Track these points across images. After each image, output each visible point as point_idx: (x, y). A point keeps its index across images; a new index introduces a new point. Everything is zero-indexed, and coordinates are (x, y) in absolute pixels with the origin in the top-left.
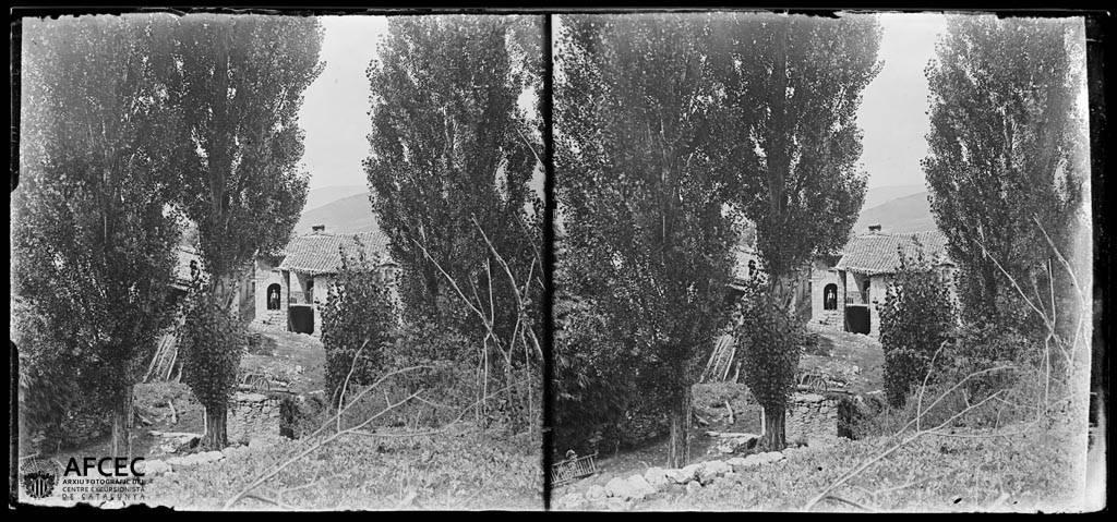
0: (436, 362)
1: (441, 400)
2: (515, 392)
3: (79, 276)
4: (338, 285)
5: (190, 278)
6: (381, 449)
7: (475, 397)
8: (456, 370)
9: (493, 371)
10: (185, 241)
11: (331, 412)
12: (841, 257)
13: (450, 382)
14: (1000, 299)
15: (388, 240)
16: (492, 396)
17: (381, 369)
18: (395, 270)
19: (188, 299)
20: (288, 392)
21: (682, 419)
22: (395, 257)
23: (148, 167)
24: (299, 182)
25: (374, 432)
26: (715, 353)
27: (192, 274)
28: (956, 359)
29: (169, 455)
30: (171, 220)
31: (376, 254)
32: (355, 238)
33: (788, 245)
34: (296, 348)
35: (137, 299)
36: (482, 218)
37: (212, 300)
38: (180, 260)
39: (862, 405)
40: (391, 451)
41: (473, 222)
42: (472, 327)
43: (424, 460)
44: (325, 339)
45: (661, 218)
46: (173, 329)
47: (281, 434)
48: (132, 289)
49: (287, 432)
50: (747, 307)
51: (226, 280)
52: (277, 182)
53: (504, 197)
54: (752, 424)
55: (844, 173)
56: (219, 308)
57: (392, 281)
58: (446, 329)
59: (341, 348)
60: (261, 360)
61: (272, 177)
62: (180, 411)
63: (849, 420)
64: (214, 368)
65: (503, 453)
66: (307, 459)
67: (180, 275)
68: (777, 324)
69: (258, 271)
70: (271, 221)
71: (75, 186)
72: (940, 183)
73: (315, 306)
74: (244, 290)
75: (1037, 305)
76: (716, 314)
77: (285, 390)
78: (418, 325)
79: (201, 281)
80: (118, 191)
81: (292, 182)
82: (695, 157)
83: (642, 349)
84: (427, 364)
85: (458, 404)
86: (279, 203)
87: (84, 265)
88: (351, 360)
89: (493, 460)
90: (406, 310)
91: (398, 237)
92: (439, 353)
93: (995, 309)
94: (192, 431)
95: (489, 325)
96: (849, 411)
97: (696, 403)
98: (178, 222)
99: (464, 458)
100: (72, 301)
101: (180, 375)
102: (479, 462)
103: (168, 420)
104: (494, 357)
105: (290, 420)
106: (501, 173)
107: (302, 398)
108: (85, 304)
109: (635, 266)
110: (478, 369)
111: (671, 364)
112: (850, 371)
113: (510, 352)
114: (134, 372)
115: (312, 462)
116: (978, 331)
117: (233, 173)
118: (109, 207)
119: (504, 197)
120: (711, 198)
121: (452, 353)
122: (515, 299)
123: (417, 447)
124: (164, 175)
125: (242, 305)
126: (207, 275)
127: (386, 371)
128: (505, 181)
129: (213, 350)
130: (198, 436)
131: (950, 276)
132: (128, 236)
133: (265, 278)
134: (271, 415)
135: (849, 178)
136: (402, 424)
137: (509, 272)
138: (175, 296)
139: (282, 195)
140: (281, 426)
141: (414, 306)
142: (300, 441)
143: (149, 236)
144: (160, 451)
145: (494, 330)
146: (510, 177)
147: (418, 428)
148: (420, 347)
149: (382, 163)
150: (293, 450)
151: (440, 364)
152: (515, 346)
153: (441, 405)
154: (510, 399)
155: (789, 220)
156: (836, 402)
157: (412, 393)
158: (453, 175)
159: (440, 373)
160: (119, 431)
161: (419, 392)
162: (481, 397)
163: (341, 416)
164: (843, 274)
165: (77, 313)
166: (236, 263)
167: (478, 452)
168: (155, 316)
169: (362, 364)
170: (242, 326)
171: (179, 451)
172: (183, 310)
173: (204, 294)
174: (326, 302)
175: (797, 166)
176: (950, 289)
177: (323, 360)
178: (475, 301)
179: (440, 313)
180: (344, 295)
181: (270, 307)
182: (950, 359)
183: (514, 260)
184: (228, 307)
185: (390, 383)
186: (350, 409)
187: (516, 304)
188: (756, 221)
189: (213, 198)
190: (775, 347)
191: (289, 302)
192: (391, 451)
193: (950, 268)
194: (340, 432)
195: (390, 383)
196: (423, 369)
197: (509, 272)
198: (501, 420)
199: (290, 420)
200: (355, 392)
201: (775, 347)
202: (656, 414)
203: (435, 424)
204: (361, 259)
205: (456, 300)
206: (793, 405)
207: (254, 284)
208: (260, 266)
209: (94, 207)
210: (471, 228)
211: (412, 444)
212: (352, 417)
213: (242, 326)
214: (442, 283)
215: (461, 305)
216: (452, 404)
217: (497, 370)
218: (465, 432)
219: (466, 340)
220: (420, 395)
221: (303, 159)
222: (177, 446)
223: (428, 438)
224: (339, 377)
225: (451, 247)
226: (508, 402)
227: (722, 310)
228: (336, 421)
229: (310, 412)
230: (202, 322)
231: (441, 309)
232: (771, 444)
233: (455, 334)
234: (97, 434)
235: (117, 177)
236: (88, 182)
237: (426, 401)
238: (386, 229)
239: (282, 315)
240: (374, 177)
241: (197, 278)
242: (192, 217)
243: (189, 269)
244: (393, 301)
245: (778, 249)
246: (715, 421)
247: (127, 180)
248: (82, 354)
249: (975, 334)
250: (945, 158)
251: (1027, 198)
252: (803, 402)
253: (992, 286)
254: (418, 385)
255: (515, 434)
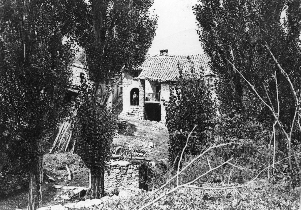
0: (242, 140)
1: (245, 165)
2: (294, 160)
3: (7, 83)
4: (177, 89)
5: (79, 84)
6: (205, 198)
7: (267, 163)
8: (254, 145)
9: (279, 146)
10: (76, 60)
11: (172, 173)
12: (142, 70)
13: (251, 153)
14: (244, 98)
15: (210, 59)
16: (278, 162)
17: (205, 144)
18: (214, 79)
19: (79, 99)
20: (144, 159)
21: (37, 178)
22: (214, 71)
23: (52, 11)
24: (151, 21)
25: (201, 186)
26: (59, 134)
27: (81, 81)
28: (215, 138)
29: (66, 201)
30: (67, 46)
31: (202, 68)
32: (188, 58)
33: (106, 63)
34: (149, 131)
35: (45, 99)
36: (271, 44)
37: (94, 99)
38: (73, 72)
39: (156, 170)
40: (212, 199)
41: (265, 47)
42: (265, 117)
43: (233, 205)
44: (168, 125)
45: (22, 45)
46: (69, 118)
47: (140, 188)
48: (42, 92)
49: (144, 186)
50: (79, 104)
51: (104, 86)
52: (137, 21)
53: (286, 30)
54: (83, 180)
55: (142, 16)
56: (99, 104)
57: (212, 86)
58: (248, 118)
59: (179, 131)
60: (126, 139)
61: (133, 18)
62: (73, 172)
63: (146, 177)
64: (95, 144)
65: (286, 201)
66: (157, 204)
67: (74, 83)
68: (98, 114)
69: (125, 80)
70: (133, 47)
71: (5, 24)
72: (205, 22)
73: (161, 103)
74: (115, 92)
75: (268, 103)
76: (59, 109)
77: (142, 158)
78: (230, 115)
79: (87, 86)
80: (33, 28)
81: (146, 21)
82: (44, 5)
83: (10, 132)
84: (236, 141)
85: (256, 168)
86: (138, 35)
87: (11, 76)
88: (185, 139)
89: (279, 205)
90: (222, 105)
91: (217, 57)
92: (243, 134)
93: (242, 104)
94: (81, 185)
95: (276, 116)
96: (146, 172)
97: (46, 166)
98: (72, 48)
99: (261, 204)
100: (3, 99)
101: (73, 149)
102: (270, 206)
103: (66, 178)
104: (280, 137)
105: (146, 178)
106: (284, 14)
107: (153, 164)
108: (12, 102)
109: (6, 78)
110: (269, 145)
111: (29, 142)
112: (147, 145)
113: (290, 134)
114: (44, 146)
115: (160, 206)
116: (229, 119)
117: (108, 15)
118: (27, 37)
119: (286, 30)
120: (55, 32)
121: (252, 134)
122: (293, 97)
123: (229, 196)
124: (63, 17)
125: (114, 102)
126: (91, 83)
127: (209, 146)
128: (287, 20)
129: (95, 132)
130: (85, 189)
131: (212, 83)
132: (39, 57)
133: (129, 84)
134: (133, 175)
135: (145, 19)
136: (219, 181)
137: (289, 80)
138: (70, 97)
139: (140, 30)
140: (139, 182)
141: (227, 103)
142: (153, 192)
143: (53, 57)
144: (61, 198)
145: (280, 119)
146: (289, 18)
147: (230, 183)
148: (230, 130)
149: (205, 8)
150: (147, 198)
151: (243, 142)
152: (293, 129)
153: (246, 169)
154: (290, 165)
155: (106, 47)
156: (138, 166)
157: (226, 161)
158: (253, 17)
159: (244, 147)
160: (34, 185)
161: (230, 160)
162: (271, 163)
163: (179, 175)
164: (143, 82)
165: (6, 108)
166: (110, 74)
167: (269, 200)
168: (57, 110)
169: (193, 141)
170: (114, 116)
171: (74, 198)
172: (76, 105)
173: (89, 95)
174: (168, 100)
175: (112, 11)
176: (212, 92)
177: (167, 139)
178: (267, 99)
179: (244, 107)
180: (181, 95)
181: (132, 104)
182: (211, 137)
183: (292, 72)
184: (105, 103)
185: (211, 154)
186: (185, 171)
187: (294, 101)
188: (85, 48)
189: (94, 32)
190: (97, 130)
191: (145, 100)
192: (212, 199)
193: (213, 78)
194: (178, 186)
195: (211, 154)
196: (233, 144)
197: (289, 80)
198: (284, 179)
199: (146, 178)
200: (188, 160)
201: (97, 130)
202: (20, 174)
203: (241, 181)
204: (192, 72)
205: (254, 99)
206: (110, 168)
207: (121, 88)
208: (126, 76)
209: (17, 38)
210: (264, 51)
211: (225, 194)
212: (186, 177)
213: (114, 116)
214: (245, 87)
215: (258, 102)
216: (252, 168)
217: (282, 146)
218: (260, 186)
219: (261, 125)
220: (231, 162)
221: (154, 6)
222: (71, 195)
223: (236, 191)
224: (178, 150)
225: (251, 64)
226: (289, 166)
227: (63, 106)
228: (175, 179)
229: (158, 173)
230: (88, 113)
231: (244, 104)
232: (94, 194)
233: (254, 122)
234: (19, 187)
235: (33, 18)
236: (13, 22)
237: (236, 166)
238: (208, 52)
239: (140, 109)
240: (200, 18)
241: (84, 84)
242: (81, 45)
243: (79, 79)
244: (213, 99)
245: (99, 66)
246: (59, 178)
247: (38, 20)
248: (9, 135)
249: (227, 121)
250: (209, 5)
251: (262, 32)
252: (116, 166)
253: (239, 89)
254: (229, 155)
255: (294, 188)
